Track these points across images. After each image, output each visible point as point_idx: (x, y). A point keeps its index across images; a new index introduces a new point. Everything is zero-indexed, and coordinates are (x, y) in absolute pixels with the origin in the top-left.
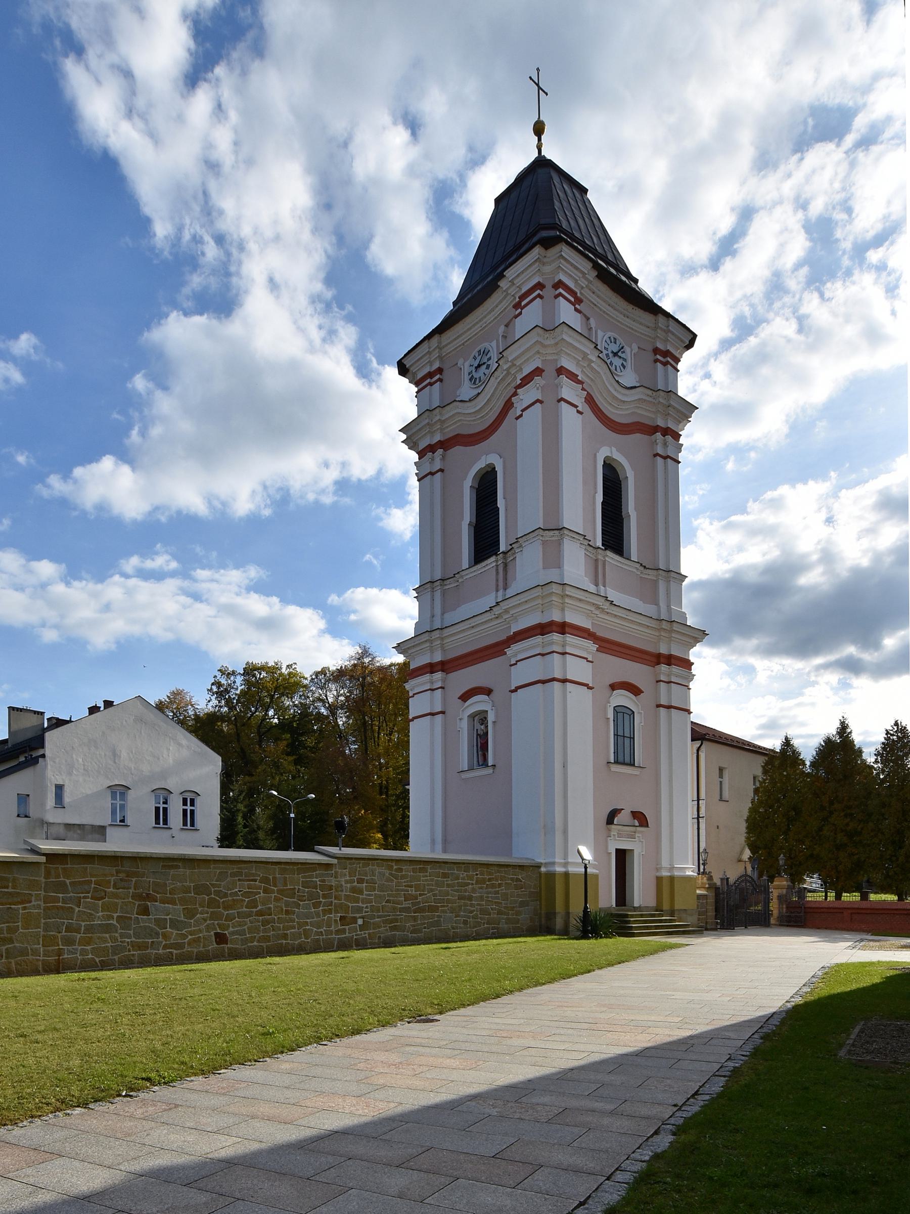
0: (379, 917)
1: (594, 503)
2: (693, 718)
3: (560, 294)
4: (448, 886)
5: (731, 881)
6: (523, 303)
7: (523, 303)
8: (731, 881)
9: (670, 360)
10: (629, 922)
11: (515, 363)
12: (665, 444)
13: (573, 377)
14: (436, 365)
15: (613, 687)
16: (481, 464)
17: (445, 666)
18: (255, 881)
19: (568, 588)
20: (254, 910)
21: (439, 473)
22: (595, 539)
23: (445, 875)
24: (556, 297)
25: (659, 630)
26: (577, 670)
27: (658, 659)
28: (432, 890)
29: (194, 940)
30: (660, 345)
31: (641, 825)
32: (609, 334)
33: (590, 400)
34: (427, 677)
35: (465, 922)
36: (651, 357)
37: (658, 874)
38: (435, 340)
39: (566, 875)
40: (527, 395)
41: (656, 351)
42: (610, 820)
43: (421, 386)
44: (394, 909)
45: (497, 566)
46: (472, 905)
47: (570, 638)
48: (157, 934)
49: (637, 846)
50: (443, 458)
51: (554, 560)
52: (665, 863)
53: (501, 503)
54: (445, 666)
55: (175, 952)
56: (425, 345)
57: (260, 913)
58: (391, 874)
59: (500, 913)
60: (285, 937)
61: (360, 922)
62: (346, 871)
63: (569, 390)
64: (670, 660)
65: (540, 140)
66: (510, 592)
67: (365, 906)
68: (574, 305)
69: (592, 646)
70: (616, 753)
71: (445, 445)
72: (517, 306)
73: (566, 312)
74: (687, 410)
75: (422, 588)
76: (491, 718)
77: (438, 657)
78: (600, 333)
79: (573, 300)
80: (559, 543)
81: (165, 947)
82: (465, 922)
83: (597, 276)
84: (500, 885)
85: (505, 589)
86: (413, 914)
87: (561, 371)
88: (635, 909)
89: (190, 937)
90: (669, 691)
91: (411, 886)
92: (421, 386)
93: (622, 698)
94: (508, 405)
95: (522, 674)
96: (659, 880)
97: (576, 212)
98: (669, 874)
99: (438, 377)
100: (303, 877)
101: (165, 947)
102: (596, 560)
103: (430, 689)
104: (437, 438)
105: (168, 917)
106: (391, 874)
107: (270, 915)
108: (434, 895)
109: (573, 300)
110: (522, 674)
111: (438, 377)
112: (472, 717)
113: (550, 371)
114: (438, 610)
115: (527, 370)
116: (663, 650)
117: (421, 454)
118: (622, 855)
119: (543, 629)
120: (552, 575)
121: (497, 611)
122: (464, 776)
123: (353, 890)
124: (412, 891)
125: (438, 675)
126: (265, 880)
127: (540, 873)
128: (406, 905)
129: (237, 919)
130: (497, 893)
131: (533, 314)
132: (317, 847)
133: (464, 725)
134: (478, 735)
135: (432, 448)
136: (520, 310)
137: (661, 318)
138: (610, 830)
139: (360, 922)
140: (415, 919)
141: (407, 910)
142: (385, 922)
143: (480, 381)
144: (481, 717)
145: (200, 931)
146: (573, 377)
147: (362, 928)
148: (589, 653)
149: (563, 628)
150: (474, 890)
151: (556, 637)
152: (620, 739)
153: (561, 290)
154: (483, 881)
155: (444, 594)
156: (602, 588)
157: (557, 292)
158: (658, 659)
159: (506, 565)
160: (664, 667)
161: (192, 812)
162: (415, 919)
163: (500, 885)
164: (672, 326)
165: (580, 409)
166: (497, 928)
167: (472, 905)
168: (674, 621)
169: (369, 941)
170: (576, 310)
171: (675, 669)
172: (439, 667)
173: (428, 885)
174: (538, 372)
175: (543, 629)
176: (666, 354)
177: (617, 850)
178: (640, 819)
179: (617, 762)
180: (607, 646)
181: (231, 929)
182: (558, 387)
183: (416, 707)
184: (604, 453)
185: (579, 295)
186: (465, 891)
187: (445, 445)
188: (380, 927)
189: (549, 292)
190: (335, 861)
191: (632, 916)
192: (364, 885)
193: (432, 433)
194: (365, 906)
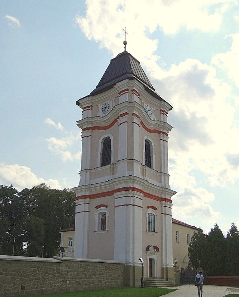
0: (74, 280)
1: (143, 152)
2: (172, 217)
3: (134, 93)
4: (96, 270)
5: (184, 269)
6: (122, 93)
7: (122, 93)
8: (184, 269)
9: (165, 113)
10: (154, 282)
11: (119, 109)
12: (164, 137)
13: (137, 116)
14: (90, 105)
15: (148, 207)
16: (106, 136)
17: (90, 197)
18: (36, 268)
19: (135, 177)
20: (35, 278)
21: (90, 136)
22: (143, 162)
23: (95, 267)
24: (132, 93)
25: (162, 191)
26: (138, 202)
27: (162, 199)
28: (91, 271)
29: (14, 288)
30: (162, 109)
31: (157, 251)
32: (147, 104)
33: (142, 123)
34: (83, 200)
35: (101, 282)
36: (160, 112)
37: (162, 267)
38: (90, 98)
39: (134, 267)
40: (122, 119)
41: (161, 110)
42: (147, 249)
43: (84, 110)
44: (79, 278)
45: (110, 168)
46: (103, 277)
47: (136, 192)
48: (2, 286)
49: (156, 257)
50: (92, 132)
51: (131, 168)
52: (164, 264)
53: (112, 149)
54: (90, 197)
55: (7, 292)
56: (87, 99)
57: (36, 279)
58: (79, 266)
59: (112, 279)
60: (44, 287)
61: (68, 282)
62: (65, 265)
63: (136, 120)
64: (165, 200)
65: (125, 46)
66: (116, 176)
67: (70, 277)
68: (138, 96)
69: (142, 195)
70: (149, 228)
71: (92, 128)
72: (119, 93)
73: (135, 98)
74: (170, 128)
75: (82, 171)
76: (107, 215)
77: (87, 193)
78: (145, 104)
79: (137, 95)
80: (132, 164)
81: (5, 290)
82: (101, 282)
83: (145, 89)
84: (112, 270)
85: (113, 175)
86: (85, 280)
87: (133, 114)
88: (155, 278)
89: (13, 287)
90: (165, 209)
91: (85, 270)
92: (84, 110)
93: (151, 211)
94: (116, 121)
95: (118, 202)
96: (162, 269)
97: (137, 69)
98: (133, 265)
99: (91, 108)
100: (51, 267)
101: (5, 290)
102: (143, 169)
103: (84, 204)
104: (90, 126)
105: (6, 280)
106: (79, 266)
107: (40, 279)
108: (92, 273)
109: (137, 95)
110: (118, 202)
111: (91, 108)
112: (99, 213)
113: (130, 113)
114: (88, 178)
115: (123, 112)
116: (163, 197)
117: (84, 130)
118: (151, 260)
119: (127, 189)
120: (130, 173)
121: (111, 182)
122: (96, 233)
123: (67, 271)
124: (85, 272)
125: (88, 199)
126: (39, 268)
127: (125, 266)
128: (83, 276)
129: (29, 281)
130: (111, 272)
131: (125, 97)
132: (54, 257)
133: (96, 216)
134: (101, 220)
135: (88, 129)
136: (120, 95)
137: (162, 102)
138: (147, 252)
139: (68, 282)
140: (85, 281)
141: (83, 278)
142: (76, 282)
143: (106, 112)
144: (104, 214)
145: (16, 285)
146: (137, 116)
147: (69, 284)
148: (141, 197)
149: (134, 189)
150: (104, 272)
151: (131, 192)
152: (150, 224)
153: (134, 92)
154: (107, 269)
155: (90, 173)
156: (145, 177)
157: (133, 92)
158: (162, 199)
159: (113, 168)
160: (164, 202)
161: (72, 242)
162: (85, 281)
163: (112, 270)
164: (166, 104)
165: (139, 125)
166: (111, 284)
167: (103, 277)
168: (167, 188)
169: (70, 289)
170: (138, 97)
171: (167, 203)
172: (88, 197)
173: (90, 270)
174: (126, 114)
175: (127, 189)
176: (164, 111)
177: (149, 259)
178: (157, 249)
179: (149, 231)
180: (147, 195)
181: (27, 284)
182: (132, 119)
183: (77, 209)
184: (146, 138)
185: (139, 93)
186: (102, 272)
187: (92, 128)
188: (74, 284)
189: (130, 92)
190: (62, 262)
191: (155, 281)
192: (70, 269)
193: (88, 124)
194: (70, 277)
